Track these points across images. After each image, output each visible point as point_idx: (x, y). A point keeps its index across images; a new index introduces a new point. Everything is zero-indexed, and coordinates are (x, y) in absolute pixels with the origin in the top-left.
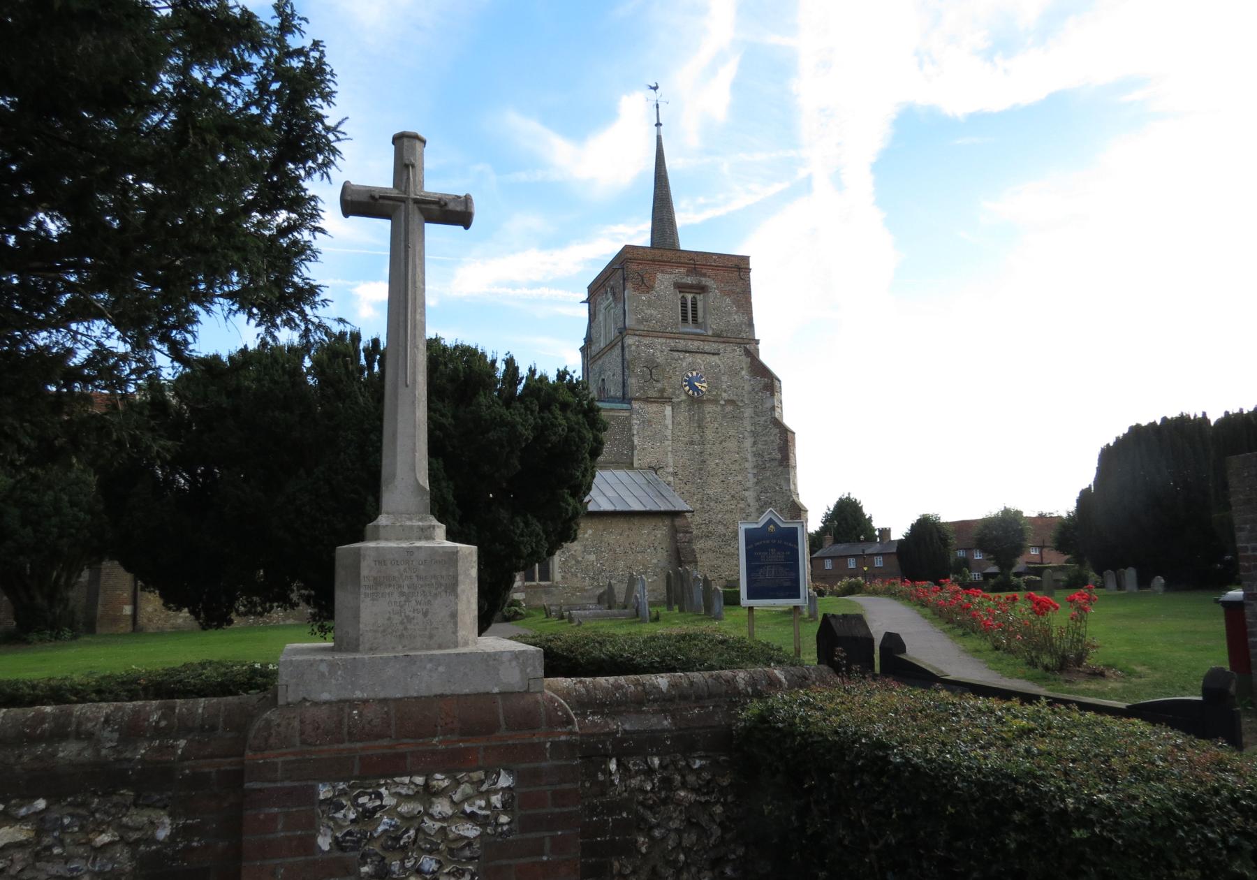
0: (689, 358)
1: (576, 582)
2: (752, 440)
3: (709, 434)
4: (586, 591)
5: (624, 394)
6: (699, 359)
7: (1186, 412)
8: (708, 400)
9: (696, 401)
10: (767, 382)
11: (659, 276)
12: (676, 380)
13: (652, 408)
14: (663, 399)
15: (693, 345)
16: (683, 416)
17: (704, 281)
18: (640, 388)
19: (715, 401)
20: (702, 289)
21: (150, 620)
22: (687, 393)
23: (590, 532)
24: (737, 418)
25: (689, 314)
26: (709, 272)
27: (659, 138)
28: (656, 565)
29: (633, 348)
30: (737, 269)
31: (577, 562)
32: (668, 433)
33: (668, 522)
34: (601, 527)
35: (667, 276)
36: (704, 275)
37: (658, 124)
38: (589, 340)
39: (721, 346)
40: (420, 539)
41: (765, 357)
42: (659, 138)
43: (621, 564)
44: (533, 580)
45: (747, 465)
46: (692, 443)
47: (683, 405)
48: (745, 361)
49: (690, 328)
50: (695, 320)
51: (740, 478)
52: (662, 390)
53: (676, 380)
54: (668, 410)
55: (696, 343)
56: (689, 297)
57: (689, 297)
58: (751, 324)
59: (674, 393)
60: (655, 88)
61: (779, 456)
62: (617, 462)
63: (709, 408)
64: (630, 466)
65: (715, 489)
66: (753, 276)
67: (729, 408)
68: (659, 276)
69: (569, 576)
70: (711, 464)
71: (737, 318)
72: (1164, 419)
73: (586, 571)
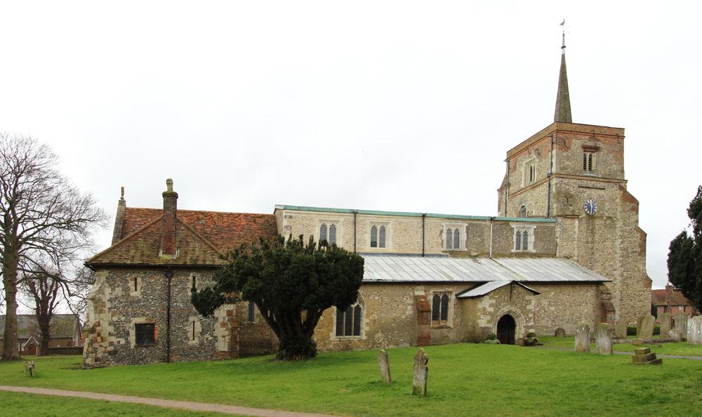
0: (588, 191)
3: (597, 238)
4: (549, 328)
5: (548, 214)
8: (598, 217)
9: (591, 217)
10: (632, 203)
11: (574, 141)
12: (581, 205)
13: (568, 221)
14: (574, 216)
15: (590, 184)
16: (584, 227)
17: (599, 144)
19: (601, 218)
20: (596, 149)
22: (586, 213)
23: (552, 293)
24: (613, 227)
25: (587, 165)
26: (602, 139)
27: (563, 56)
28: (587, 313)
30: (617, 136)
31: (545, 311)
32: (576, 236)
33: (594, 288)
35: (578, 141)
36: (599, 140)
37: (563, 47)
38: (506, 185)
39: (607, 184)
41: (631, 189)
42: (563, 56)
46: (587, 242)
47: (584, 220)
48: (619, 193)
49: (588, 174)
50: (590, 169)
52: (574, 211)
53: (581, 205)
54: (577, 222)
56: (588, 154)
58: (623, 171)
59: (579, 213)
61: (639, 250)
64: (554, 256)
66: (626, 141)
67: (608, 222)
68: (574, 141)
70: (597, 255)
71: (615, 167)
72: (670, 248)
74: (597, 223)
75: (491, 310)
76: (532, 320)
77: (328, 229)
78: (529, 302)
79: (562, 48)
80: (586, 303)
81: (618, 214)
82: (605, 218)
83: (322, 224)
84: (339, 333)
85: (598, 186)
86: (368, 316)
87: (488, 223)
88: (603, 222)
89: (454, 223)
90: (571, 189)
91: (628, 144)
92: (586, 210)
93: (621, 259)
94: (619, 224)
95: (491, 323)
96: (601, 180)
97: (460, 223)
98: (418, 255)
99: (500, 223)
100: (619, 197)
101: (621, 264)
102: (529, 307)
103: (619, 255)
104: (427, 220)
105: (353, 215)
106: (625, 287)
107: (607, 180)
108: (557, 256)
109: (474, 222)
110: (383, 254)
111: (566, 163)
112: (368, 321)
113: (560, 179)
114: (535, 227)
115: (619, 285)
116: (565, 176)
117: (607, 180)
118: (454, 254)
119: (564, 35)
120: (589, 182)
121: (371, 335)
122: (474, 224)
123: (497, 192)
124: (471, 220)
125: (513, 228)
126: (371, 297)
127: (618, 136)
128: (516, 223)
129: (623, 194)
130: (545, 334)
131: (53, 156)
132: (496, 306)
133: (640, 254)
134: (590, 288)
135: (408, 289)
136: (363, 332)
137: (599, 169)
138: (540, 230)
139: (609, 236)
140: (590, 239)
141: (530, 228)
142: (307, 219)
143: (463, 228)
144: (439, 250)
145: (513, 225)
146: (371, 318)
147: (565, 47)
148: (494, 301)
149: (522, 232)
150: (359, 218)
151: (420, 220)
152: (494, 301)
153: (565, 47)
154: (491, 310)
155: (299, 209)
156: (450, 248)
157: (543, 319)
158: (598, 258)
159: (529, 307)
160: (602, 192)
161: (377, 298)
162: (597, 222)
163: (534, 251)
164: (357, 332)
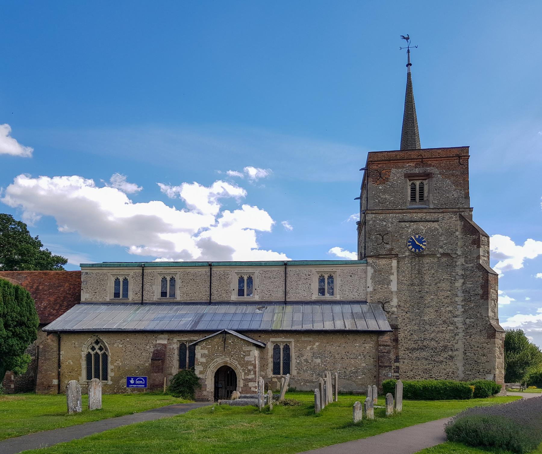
0: (414, 226)
2: (461, 281)
3: (427, 278)
7: (484, 453)
11: (394, 170)
14: (390, 255)
15: (416, 216)
16: (406, 264)
17: (429, 169)
18: (374, 249)
19: (433, 255)
20: (428, 176)
22: (410, 250)
24: (452, 265)
25: (418, 195)
27: (409, 75)
29: (371, 222)
33: (374, 338)
34: (325, 341)
36: (430, 165)
37: (409, 65)
40: (189, 352)
42: (409, 75)
43: (339, 366)
44: (279, 374)
45: (457, 299)
46: (412, 285)
48: (459, 224)
51: (450, 308)
54: (394, 263)
55: (420, 215)
56: (418, 183)
57: (418, 183)
60: (407, 39)
61: (481, 292)
63: (427, 260)
65: (429, 315)
67: (444, 259)
68: (394, 170)
69: (302, 372)
70: (428, 299)
73: (314, 370)
76: (252, 372)
77: (168, 282)
78: (248, 353)
79: (407, 66)
80: (361, 353)
83: (239, 276)
85: (428, 217)
86: (112, 363)
88: (436, 260)
91: (475, 166)
93: (463, 304)
94: (461, 261)
95: (203, 374)
96: (434, 211)
100: (459, 228)
101: (463, 310)
102: (247, 359)
103: (462, 299)
105: (141, 268)
111: (382, 197)
112: (113, 367)
113: (374, 215)
115: (461, 335)
117: (441, 210)
119: (408, 51)
120: (415, 215)
123: (208, 236)
127: (459, 157)
129: (464, 226)
133: (482, 297)
136: (109, 378)
137: (431, 198)
140: (416, 281)
143: (132, 274)
146: (115, 364)
147: (411, 65)
151: (282, 269)
152: (206, 352)
153: (411, 65)
155: (93, 265)
159: (247, 359)
160: (435, 225)
161: (121, 346)
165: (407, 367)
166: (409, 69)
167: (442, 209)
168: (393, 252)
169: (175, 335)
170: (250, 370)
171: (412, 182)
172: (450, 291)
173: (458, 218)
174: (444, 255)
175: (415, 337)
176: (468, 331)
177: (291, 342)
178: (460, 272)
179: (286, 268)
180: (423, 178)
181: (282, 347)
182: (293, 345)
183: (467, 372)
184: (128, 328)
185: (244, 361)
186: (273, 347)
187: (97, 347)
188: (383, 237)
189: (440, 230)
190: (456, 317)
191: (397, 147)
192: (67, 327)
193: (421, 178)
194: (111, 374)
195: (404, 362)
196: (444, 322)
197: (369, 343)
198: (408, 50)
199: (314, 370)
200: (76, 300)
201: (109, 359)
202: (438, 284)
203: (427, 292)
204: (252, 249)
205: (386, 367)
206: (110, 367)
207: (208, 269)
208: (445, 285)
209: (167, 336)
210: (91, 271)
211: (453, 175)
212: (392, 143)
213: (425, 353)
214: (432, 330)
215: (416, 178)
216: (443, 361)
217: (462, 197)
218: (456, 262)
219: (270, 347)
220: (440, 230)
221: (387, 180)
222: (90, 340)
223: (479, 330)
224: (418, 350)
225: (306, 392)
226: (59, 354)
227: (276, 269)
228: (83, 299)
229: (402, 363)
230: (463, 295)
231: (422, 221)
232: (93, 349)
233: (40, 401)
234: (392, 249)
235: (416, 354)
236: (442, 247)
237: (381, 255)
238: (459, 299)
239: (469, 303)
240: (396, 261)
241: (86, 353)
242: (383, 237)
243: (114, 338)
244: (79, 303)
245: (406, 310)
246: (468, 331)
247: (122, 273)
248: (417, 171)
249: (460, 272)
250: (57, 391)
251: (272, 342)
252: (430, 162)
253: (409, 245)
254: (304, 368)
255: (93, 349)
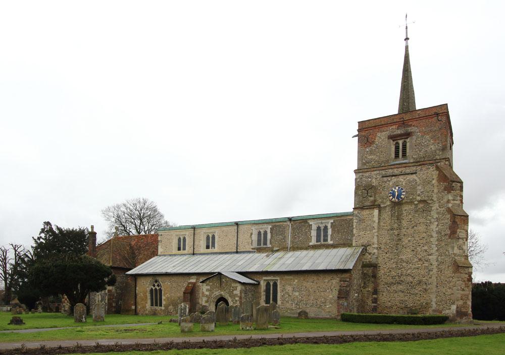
0: (394, 179)
1: (288, 305)
3: (404, 223)
6: (401, 179)
8: (406, 203)
11: (379, 134)
14: (373, 206)
15: (396, 171)
16: (387, 214)
17: (410, 129)
19: (411, 202)
20: (408, 135)
21: (140, 311)
22: (391, 201)
23: (296, 281)
25: (401, 152)
27: (407, 47)
31: (289, 296)
32: (376, 225)
36: (411, 126)
37: (407, 39)
42: (407, 47)
46: (392, 229)
47: (387, 208)
48: (435, 174)
51: (426, 248)
54: (376, 212)
55: (400, 170)
56: (401, 142)
57: (401, 142)
62: (344, 244)
65: (406, 255)
67: (421, 205)
68: (379, 134)
70: (405, 241)
73: (293, 300)
74: (406, 208)
75: (207, 293)
76: (238, 302)
79: (405, 40)
81: (435, 196)
82: (416, 203)
84: (152, 305)
86: (164, 296)
87: (288, 223)
88: (413, 206)
89: (261, 226)
90: (374, 180)
92: (391, 197)
94: (435, 206)
96: (413, 164)
97: (265, 226)
98: (234, 253)
99: (299, 222)
100: (435, 177)
101: (437, 248)
102: (235, 292)
104: (240, 227)
106: (439, 273)
107: (419, 164)
108: (354, 245)
109: (277, 224)
110: (211, 253)
111: (368, 157)
113: (361, 174)
114: (332, 221)
115: (435, 270)
116: (366, 170)
117: (419, 164)
118: (259, 250)
119: (407, 28)
120: (395, 170)
121: (167, 307)
122: (343, 220)
124: (272, 223)
125: (311, 225)
126: (166, 283)
128: (313, 220)
130: (289, 315)
131: (161, 216)
132: (211, 291)
134: (335, 276)
135: (186, 278)
136: (163, 305)
138: (337, 223)
139: (422, 220)
140: (396, 226)
141: (328, 223)
142: (169, 236)
144: (249, 248)
145: (311, 222)
148: (209, 287)
149: (322, 227)
150: (197, 231)
152: (209, 287)
154: (207, 293)
156: (261, 245)
157: (288, 302)
158: (406, 244)
159: (235, 292)
161: (169, 284)
162: (406, 208)
163: (332, 242)
164: (161, 305)
165: (386, 299)
166: (407, 43)
167: (420, 163)
168: (376, 203)
169: (326, 276)
170: (236, 301)
171: (396, 142)
172: (425, 233)
173: (435, 168)
174: (420, 201)
175: (393, 273)
176: (440, 267)
177: (277, 280)
178: (436, 216)
179: (238, 227)
180: (406, 137)
181: (271, 284)
182: (279, 281)
183: (438, 303)
184: (161, 271)
185: (233, 294)
186: (265, 284)
187: (156, 284)
188: (367, 191)
189: (418, 180)
190: (430, 255)
191: (395, 111)
192: (140, 272)
193: (403, 137)
194: (164, 303)
195: (383, 295)
196: (420, 260)
197: (334, 279)
198: (407, 27)
199: (293, 300)
200: (155, 253)
201: (163, 292)
202: (415, 227)
203: (404, 235)
204: (33, 238)
205: (343, 298)
206: (163, 298)
207: (236, 227)
208: (422, 228)
209: (196, 277)
210: (164, 233)
211: (431, 131)
212: (391, 107)
213: (401, 287)
214: (409, 267)
215: (399, 138)
216: (417, 294)
217: (439, 150)
218: (431, 207)
219: (263, 284)
220: (418, 180)
221: (373, 142)
222: (150, 279)
223: (447, 266)
224: (395, 284)
225: (325, 319)
226: (136, 290)
227: (230, 228)
228: (159, 253)
229: (381, 295)
230: (437, 235)
231: (402, 175)
232: (154, 286)
233: (475, 351)
234: (375, 201)
235: (394, 288)
236: (419, 196)
237: (365, 206)
238: (434, 240)
239: (441, 243)
240: (377, 211)
241: (150, 288)
242: (367, 191)
243: (167, 279)
244: (157, 255)
245: (386, 251)
246: (440, 267)
247: (181, 233)
248: (399, 132)
249: (436, 216)
250: (134, 313)
251: (264, 280)
252: (410, 123)
253: (390, 196)
254: (287, 300)
255: (154, 286)
